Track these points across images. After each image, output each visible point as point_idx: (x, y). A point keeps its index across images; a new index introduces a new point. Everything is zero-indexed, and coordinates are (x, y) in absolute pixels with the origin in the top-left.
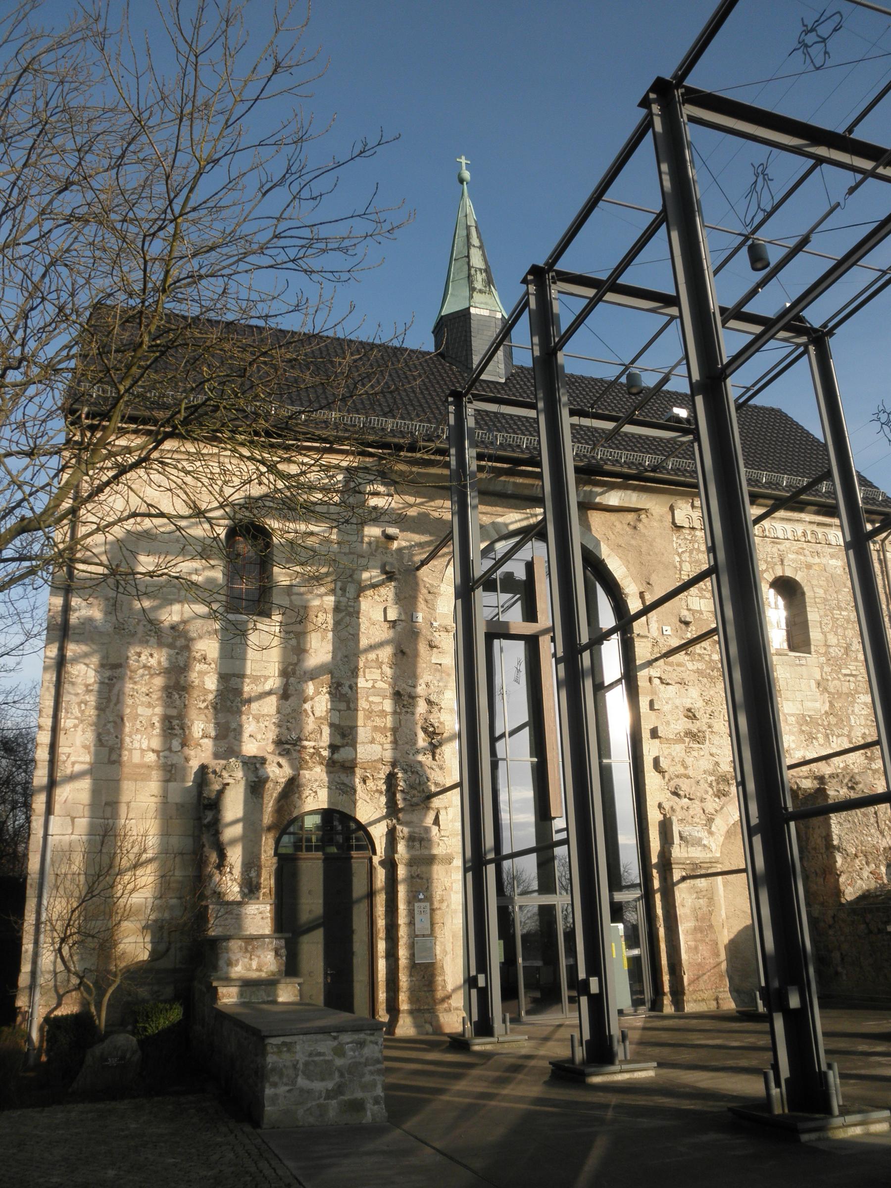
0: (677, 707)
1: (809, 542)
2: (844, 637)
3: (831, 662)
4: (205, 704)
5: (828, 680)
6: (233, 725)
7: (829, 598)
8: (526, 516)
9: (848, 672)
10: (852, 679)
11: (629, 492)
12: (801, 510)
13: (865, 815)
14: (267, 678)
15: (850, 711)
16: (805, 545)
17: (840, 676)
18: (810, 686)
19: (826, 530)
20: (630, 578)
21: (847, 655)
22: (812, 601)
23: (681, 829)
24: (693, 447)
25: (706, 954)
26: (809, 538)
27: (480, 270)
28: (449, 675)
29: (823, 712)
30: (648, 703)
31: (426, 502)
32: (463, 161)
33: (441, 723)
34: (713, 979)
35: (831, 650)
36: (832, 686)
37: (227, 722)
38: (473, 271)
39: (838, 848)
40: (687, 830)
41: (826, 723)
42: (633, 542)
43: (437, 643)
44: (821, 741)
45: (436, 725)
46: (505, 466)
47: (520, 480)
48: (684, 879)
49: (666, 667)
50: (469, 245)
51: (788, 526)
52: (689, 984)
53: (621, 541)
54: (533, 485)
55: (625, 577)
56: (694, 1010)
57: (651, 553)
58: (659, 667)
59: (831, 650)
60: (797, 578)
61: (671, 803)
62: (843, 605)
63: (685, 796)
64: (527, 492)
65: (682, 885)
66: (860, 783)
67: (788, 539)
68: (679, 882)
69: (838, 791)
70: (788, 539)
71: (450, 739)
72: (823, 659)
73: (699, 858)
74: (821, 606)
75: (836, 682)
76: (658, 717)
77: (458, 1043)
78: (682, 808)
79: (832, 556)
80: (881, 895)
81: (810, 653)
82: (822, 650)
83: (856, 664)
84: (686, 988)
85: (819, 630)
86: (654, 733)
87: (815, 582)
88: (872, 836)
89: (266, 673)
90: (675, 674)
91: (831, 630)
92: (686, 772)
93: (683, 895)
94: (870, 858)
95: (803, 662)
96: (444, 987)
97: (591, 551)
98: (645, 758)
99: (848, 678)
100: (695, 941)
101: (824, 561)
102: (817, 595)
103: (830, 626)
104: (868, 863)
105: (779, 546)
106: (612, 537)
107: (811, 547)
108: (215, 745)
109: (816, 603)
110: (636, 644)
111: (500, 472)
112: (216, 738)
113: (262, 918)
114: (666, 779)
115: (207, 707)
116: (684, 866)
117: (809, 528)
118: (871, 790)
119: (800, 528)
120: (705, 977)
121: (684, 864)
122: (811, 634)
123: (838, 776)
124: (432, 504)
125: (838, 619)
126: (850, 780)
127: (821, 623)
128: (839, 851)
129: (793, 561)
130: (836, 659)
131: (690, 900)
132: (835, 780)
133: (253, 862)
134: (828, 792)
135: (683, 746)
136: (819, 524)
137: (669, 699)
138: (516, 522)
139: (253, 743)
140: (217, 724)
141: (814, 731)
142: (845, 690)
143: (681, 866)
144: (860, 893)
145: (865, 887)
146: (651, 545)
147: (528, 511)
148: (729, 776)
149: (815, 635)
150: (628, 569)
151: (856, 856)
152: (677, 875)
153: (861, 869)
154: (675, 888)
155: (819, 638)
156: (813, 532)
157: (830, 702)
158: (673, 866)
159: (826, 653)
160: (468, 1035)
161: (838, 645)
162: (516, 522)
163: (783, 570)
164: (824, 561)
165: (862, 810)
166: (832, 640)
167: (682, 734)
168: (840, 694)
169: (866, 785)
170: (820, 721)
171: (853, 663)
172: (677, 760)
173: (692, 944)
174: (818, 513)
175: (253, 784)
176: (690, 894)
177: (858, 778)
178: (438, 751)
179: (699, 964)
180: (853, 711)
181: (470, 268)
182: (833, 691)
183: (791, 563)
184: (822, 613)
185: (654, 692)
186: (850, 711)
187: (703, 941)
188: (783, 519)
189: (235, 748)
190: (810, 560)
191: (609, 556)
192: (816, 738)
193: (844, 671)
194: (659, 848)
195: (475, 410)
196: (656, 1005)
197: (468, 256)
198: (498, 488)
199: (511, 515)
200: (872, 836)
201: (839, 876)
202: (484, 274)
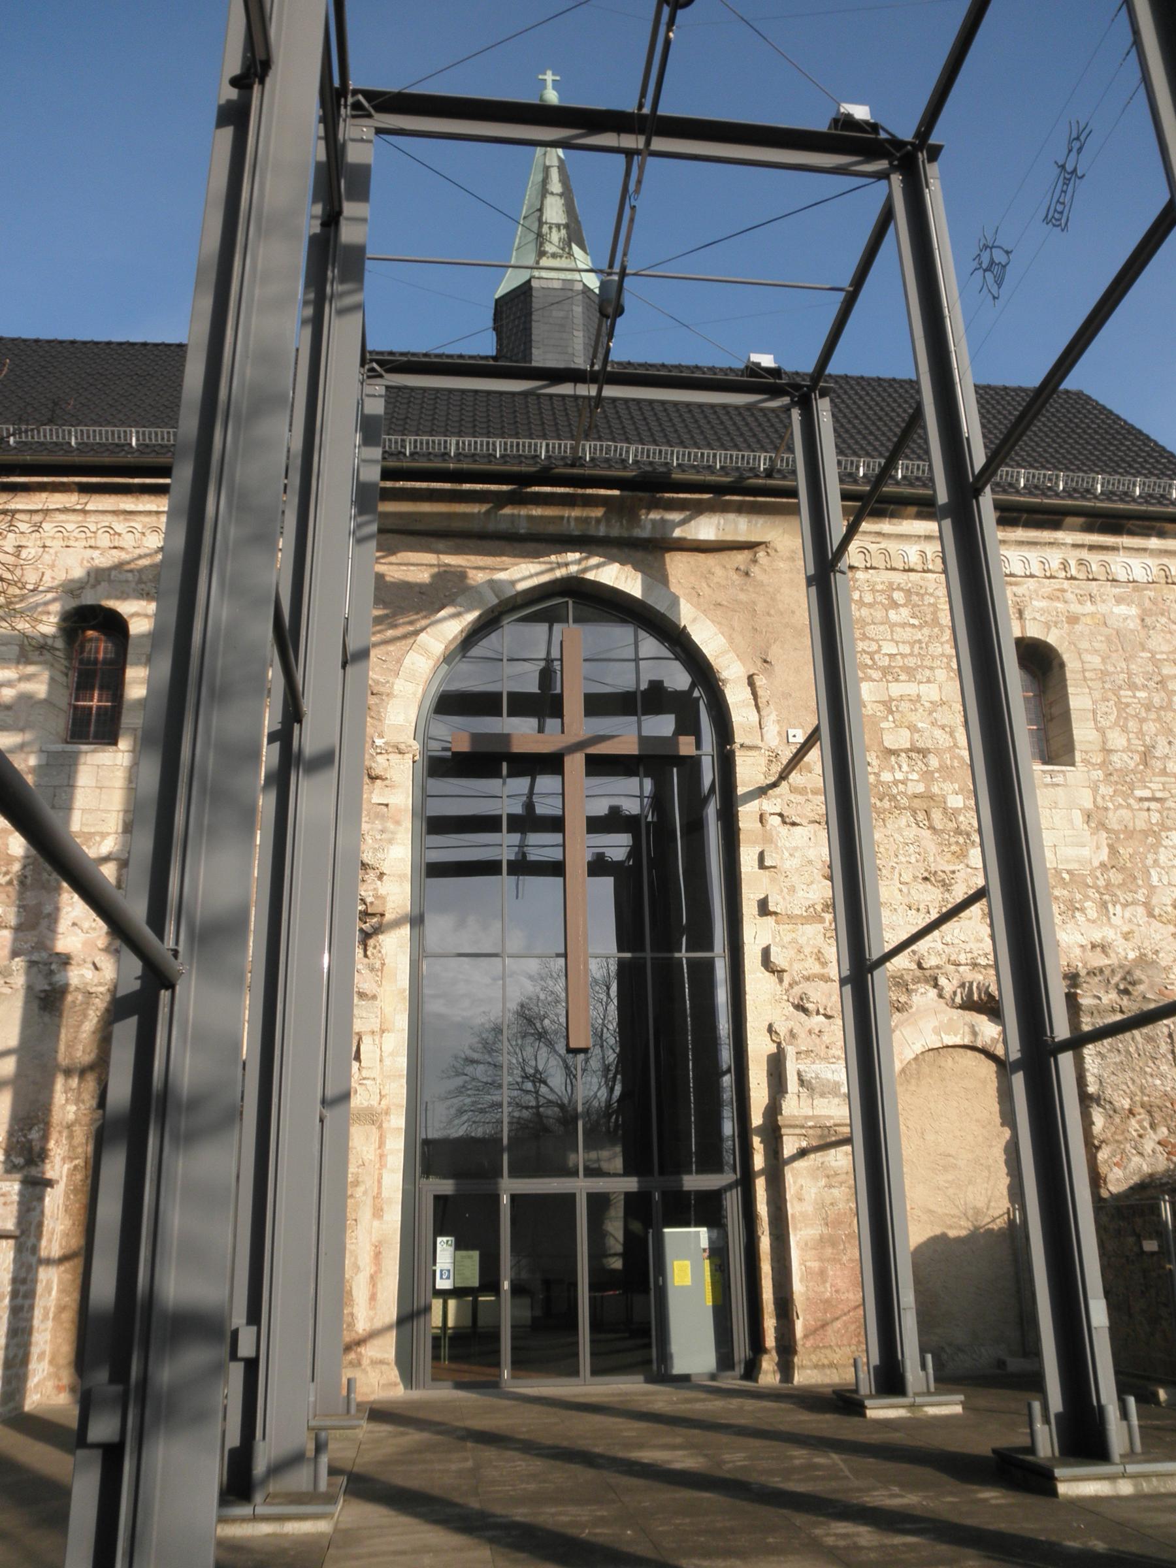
0: (810, 862)
1: (1073, 578)
2: (1141, 734)
3: (1115, 778)
4: (8, 878)
5: (1106, 809)
6: (48, 909)
7: (1111, 669)
8: (548, 566)
9: (1147, 793)
10: (1154, 805)
11: (731, 516)
12: (1056, 526)
13: (1150, 1039)
14: (104, 835)
15: (1149, 862)
16: (1066, 584)
17: (1131, 801)
18: (1071, 821)
19: (1108, 557)
20: (732, 655)
21: (1146, 765)
22: (1079, 676)
23: (802, 1067)
24: (790, 417)
25: (841, 1284)
26: (1074, 572)
27: (558, 226)
28: (398, 823)
29: (1096, 864)
30: (756, 857)
31: (383, 557)
32: (549, 77)
33: (377, 897)
34: (853, 1327)
35: (1115, 758)
36: (1114, 819)
37: (40, 905)
38: (545, 229)
39: (1096, 1099)
40: (812, 1069)
41: (1101, 883)
42: (743, 597)
43: (378, 771)
44: (1092, 913)
45: (369, 900)
46: (505, 488)
47: (537, 511)
48: (803, 1153)
49: (792, 797)
50: (544, 192)
51: (1033, 555)
52: (806, 1336)
53: (722, 597)
54: (562, 518)
55: (724, 653)
56: (813, 1381)
57: (772, 612)
58: (780, 796)
59: (1115, 758)
60: (1051, 640)
61: (791, 1024)
62: (1139, 681)
63: (818, 1013)
64: (552, 529)
65: (800, 1164)
66: (1140, 982)
67: (1032, 576)
68: (794, 1158)
69: (1100, 998)
70: (1032, 576)
71: (396, 924)
72: (1099, 774)
73: (830, 1117)
74: (1097, 685)
75: (1123, 812)
76: (773, 880)
77: (846, 1403)
78: (810, 1032)
79: (1119, 600)
80: (1168, 1183)
81: (1073, 764)
82: (1097, 758)
83: (1163, 779)
84: (799, 1342)
85: (1092, 724)
86: (764, 908)
87: (1084, 645)
88: (1162, 1076)
89: (104, 829)
90: (809, 806)
91: (1116, 724)
92: (825, 971)
93: (801, 1181)
94: (1158, 1116)
95: (1059, 779)
96: (351, 1325)
97: (663, 615)
98: (746, 948)
99: (1146, 804)
100: (821, 1260)
101: (1102, 608)
102: (1087, 666)
103: (1113, 718)
104: (1153, 1126)
105: (1015, 588)
106: (706, 591)
107: (1078, 587)
108: (15, 940)
109: (1085, 679)
110: (739, 760)
111: (501, 500)
112: (18, 929)
113: (5, 1204)
114: (786, 983)
115: (10, 883)
116: (804, 1131)
117: (1073, 556)
118: (1161, 993)
119: (1055, 558)
120: (838, 1324)
121: (802, 1127)
122: (1075, 732)
123: (1101, 971)
124: (393, 559)
125: (1128, 705)
126: (1124, 979)
127: (1094, 712)
128: (1099, 1105)
129: (1043, 611)
130: (1123, 772)
131: (814, 1190)
132: (1096, 979)
133: (37, 1117)
134: (1081, 1001)
135: (820, 927)
136: (1092, 548)
137: (796, 848)
138: (531, 576)
139: (77, 935)
140: (22, 908)
141: (1078, 896)
142: (1141, 824)
143: (798, 1131)
144: (1136, 1179)
145: (1146, 1169)
146: (773, 599)
147: (553, 558)
148: (908, 978)
149: (1083, 733)
150: (731, 640)
151: (1131, 1112)
152: (789, 1147)
153: (1140, 1136)
154: (786, 1168)
155: (1090, 738)
156: (1081, 562)
157: (1111, 847)
158: (783, 1131)
159: (1103, 764)
160: (864, 1389)
161: (1128, 749)
162: (531, 576)
163: (1023, 628)
164: (1102, 608)
165: (1145, 1030)
166: (1117, 740)
167: (819, 908)
168: (1130, 834)
169: (1152, 987)
170: (1089, 881)
171: (1157, 779)
172: (807, 951)
173: (815, 1265)
174: (1088, 529)
175: (42, 995)
176: (816, 1179)
177: (1138, 974)
178: (371, 942)
179: (827, 1302)
180: (1155, 861)
181: (541, 223)
182: (1116, 827)
183: (1037, 616)
184: (1097, 695)
185: (768, 839)
186: (1149, 862)
187: (835, 1260)
188: (1021, 543)
189: (48, 943)
190: (1075, 608)
191: (694, 620)
192: (1082, 910)
193: (1139, 793)
194: (766, 1101)
195: (387, 387)
196: (752, 1370)
197: (541, 210)
198: (503, 526)
199: (523, 566)
200: (1162, 1076)
201: (1098, 1148)
202: (563, 232)
